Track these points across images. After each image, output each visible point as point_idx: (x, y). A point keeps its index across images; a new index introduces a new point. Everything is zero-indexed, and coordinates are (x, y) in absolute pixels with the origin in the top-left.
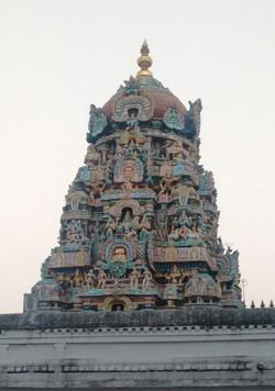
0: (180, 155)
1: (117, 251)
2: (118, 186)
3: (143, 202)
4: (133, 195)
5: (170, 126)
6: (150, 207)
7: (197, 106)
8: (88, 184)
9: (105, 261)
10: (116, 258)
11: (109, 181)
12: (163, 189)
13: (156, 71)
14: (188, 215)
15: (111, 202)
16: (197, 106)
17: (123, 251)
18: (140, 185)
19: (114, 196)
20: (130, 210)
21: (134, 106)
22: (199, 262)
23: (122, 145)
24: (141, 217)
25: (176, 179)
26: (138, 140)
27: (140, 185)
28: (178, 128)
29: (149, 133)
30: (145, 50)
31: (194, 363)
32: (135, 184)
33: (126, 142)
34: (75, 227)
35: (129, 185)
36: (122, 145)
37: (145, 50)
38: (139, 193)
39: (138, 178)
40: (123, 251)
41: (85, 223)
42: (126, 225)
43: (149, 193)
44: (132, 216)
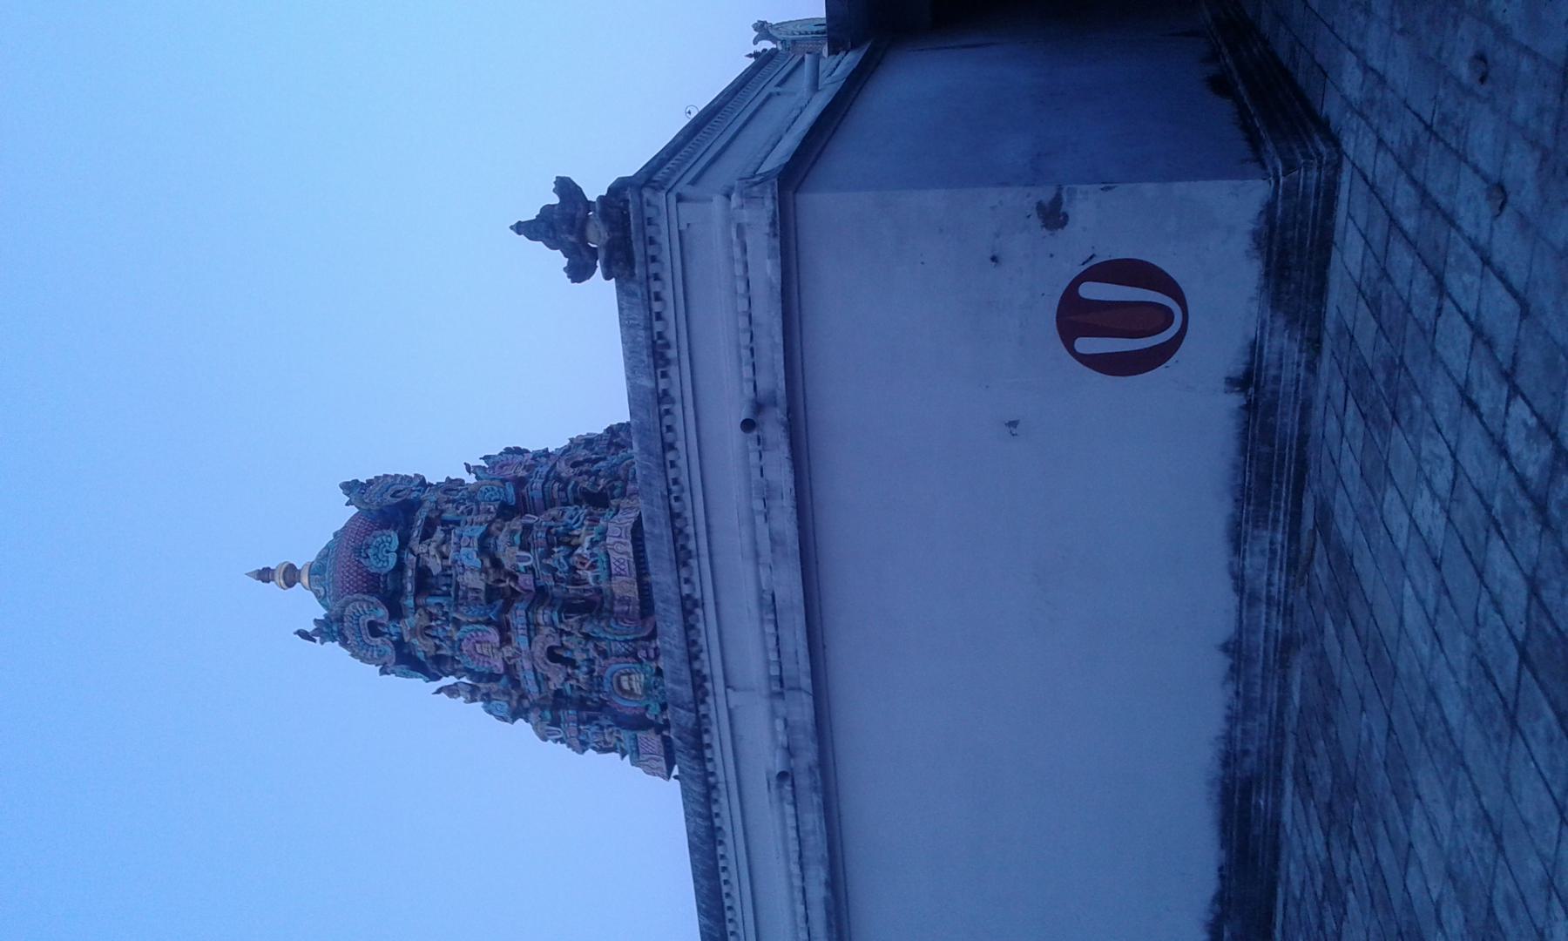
0: (444, 549)
1: (626, 686)
2: (509, 669)
3: (532, 628)
4: (524, 646)
5: (392, 560)
6: (542, 616)
7: (352, 489)
8: (514, 703)
9: (647, 708)
10: (638, 689)
11: (504, 680)
12: (508, 582)
13: (304, 557)
14: (549, 553)
15: (542, 680)
16: (352, 489)
17: (625, 678)
18: (504, 630)
19: (531, 676)
20: (551, 649)
21: (365, 631)
22: (633, 542)
23: (438, 647)
24: (562, 632)
25: (487, 563)
26: (425, 622)
27: (504, 630)
28: (396, 543)
29: (410, 602)
30: (265, 575)
31: (788, 859)
32: (505, 640)
33: (431, 642)
34: (625, 305)
35: (508, 651)
36: (438, 647)
37: (265, 575)
38: (520, 641)
39: (494, 636)
40: (625, 678)
41: (584, 715)
42: (579, 657)
43: (517, 617)
44: (563, 646)
